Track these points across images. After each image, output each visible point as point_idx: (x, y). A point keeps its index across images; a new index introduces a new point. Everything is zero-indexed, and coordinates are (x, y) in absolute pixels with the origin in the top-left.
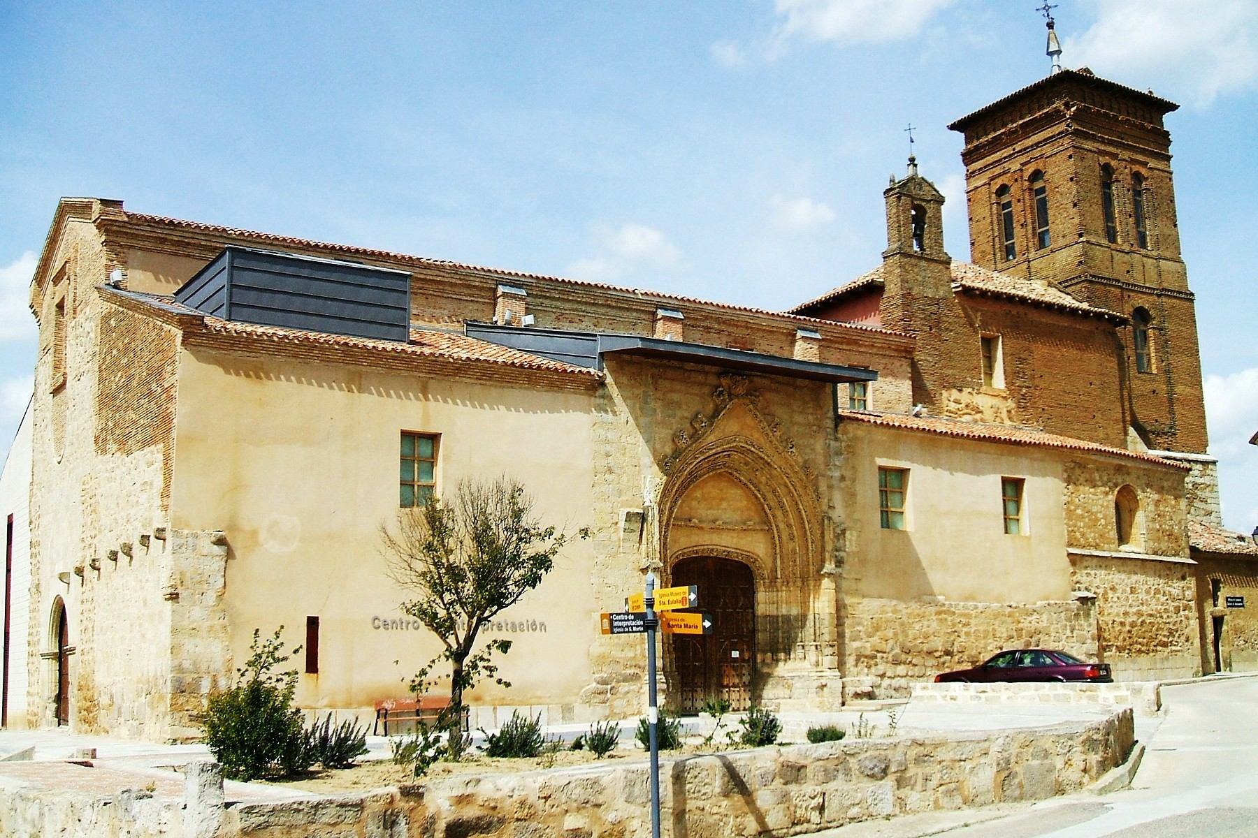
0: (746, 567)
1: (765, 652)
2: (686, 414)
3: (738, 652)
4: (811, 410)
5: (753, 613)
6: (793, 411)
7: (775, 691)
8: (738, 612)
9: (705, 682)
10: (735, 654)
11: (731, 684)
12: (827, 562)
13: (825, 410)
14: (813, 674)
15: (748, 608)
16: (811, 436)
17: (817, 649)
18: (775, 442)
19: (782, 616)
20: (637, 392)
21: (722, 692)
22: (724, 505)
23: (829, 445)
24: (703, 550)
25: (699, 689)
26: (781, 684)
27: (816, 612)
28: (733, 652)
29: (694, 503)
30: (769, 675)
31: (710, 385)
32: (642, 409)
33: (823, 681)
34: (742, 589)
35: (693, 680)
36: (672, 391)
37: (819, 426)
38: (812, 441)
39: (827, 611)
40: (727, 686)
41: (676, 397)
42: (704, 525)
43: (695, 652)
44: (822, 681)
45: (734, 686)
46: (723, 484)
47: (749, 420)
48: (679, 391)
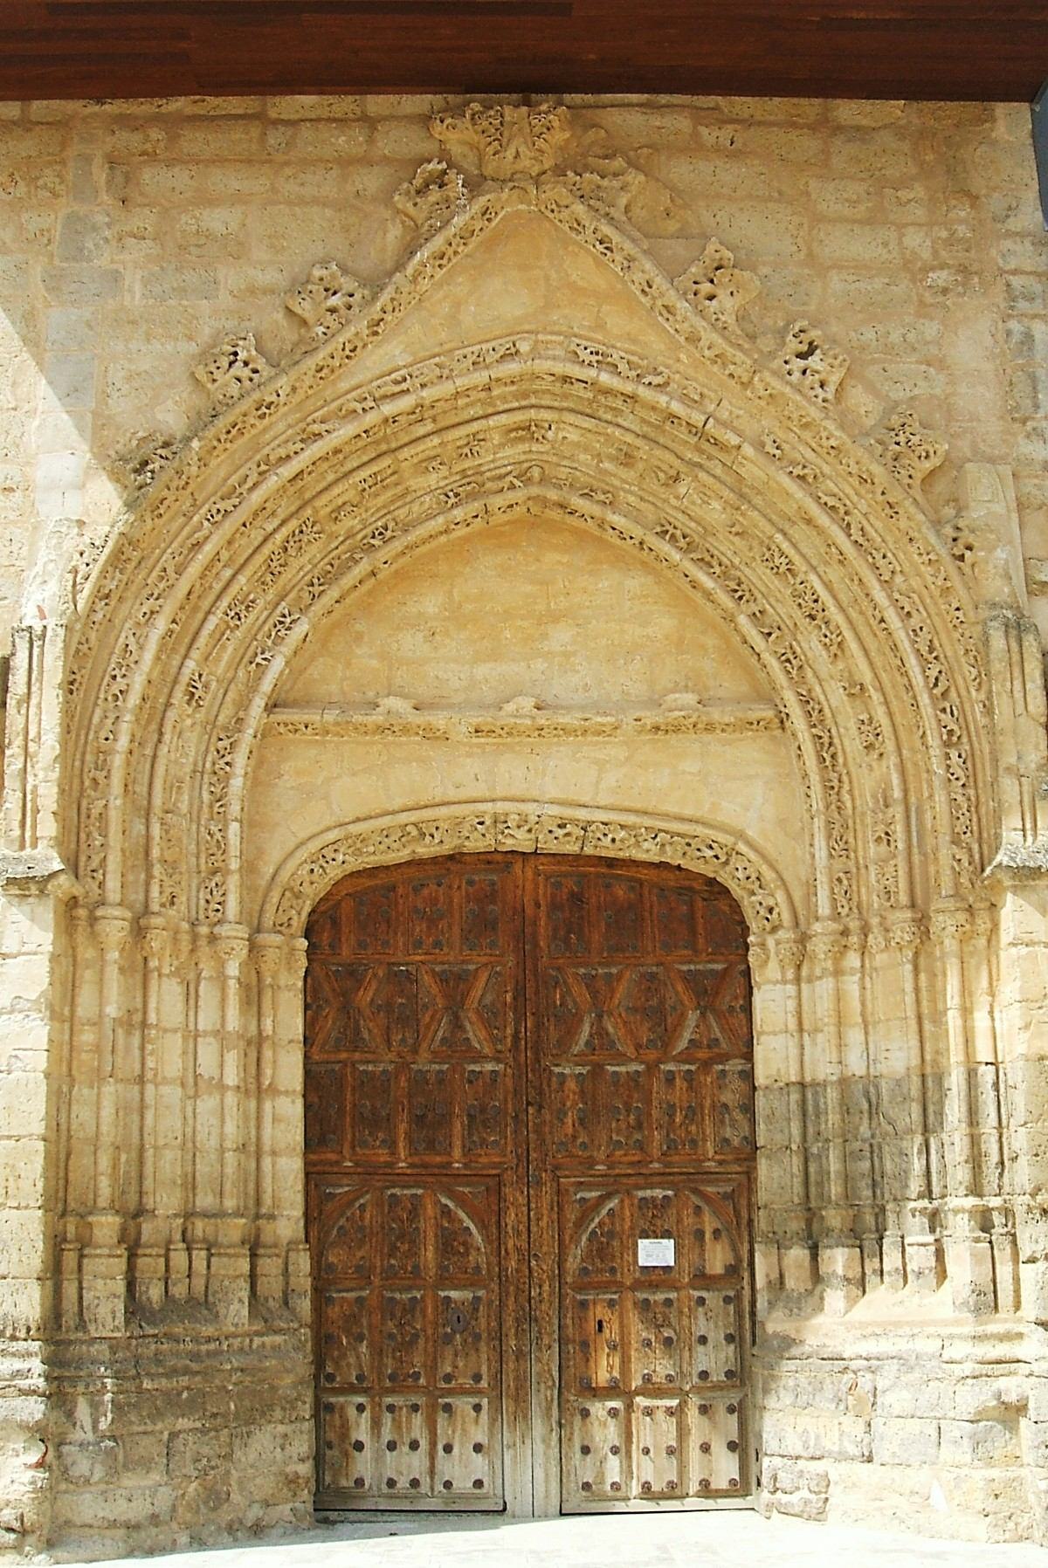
0: (716, 889)
1: (780, 1244)
2: (269, 277)
3: (669, 1244)
4: (920, 213)
5: (748, 1076)
6: (818, 219)
7: (805, 1421)
8: (670, 1079)
9: (498, 1378)
10: (656, 1252)
11: (636, 1383)
12: (1012, 821)
13: (996, 203)
14: (957, 1350)
15: (724, 1058)
16: (923, 310)
17: (986, 1227)
18: (708, 336)
19: (844, 1082)
20: (34, 221)
21: (585, 1414)
22: (561, 636)
23: (1028, 338)
24: (459, 822)
25: (463, 1404)
26: (829, 1391)
27: (984, 1054)
28: (643, 1244)
29: (411, 643)
30: (788, 1342)
31: (386, 160)
32: (54, 282)
33: (1012, 1387)
34: (690, 979)
35: (432, 1368)
36: (207, 200)
37: (964, 270)
38: (931, 329)
39: (1021, 1049)
40: (613, 1390)
41: (217, 220)
42: (439, 720)
43: (452, 1242)
44: (1002, 1383)
45: (651, 1388)
46: (551, 557)
47: (583, 269)
48: (238, 199)
